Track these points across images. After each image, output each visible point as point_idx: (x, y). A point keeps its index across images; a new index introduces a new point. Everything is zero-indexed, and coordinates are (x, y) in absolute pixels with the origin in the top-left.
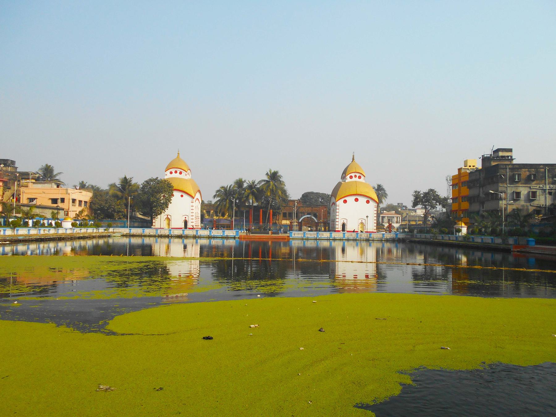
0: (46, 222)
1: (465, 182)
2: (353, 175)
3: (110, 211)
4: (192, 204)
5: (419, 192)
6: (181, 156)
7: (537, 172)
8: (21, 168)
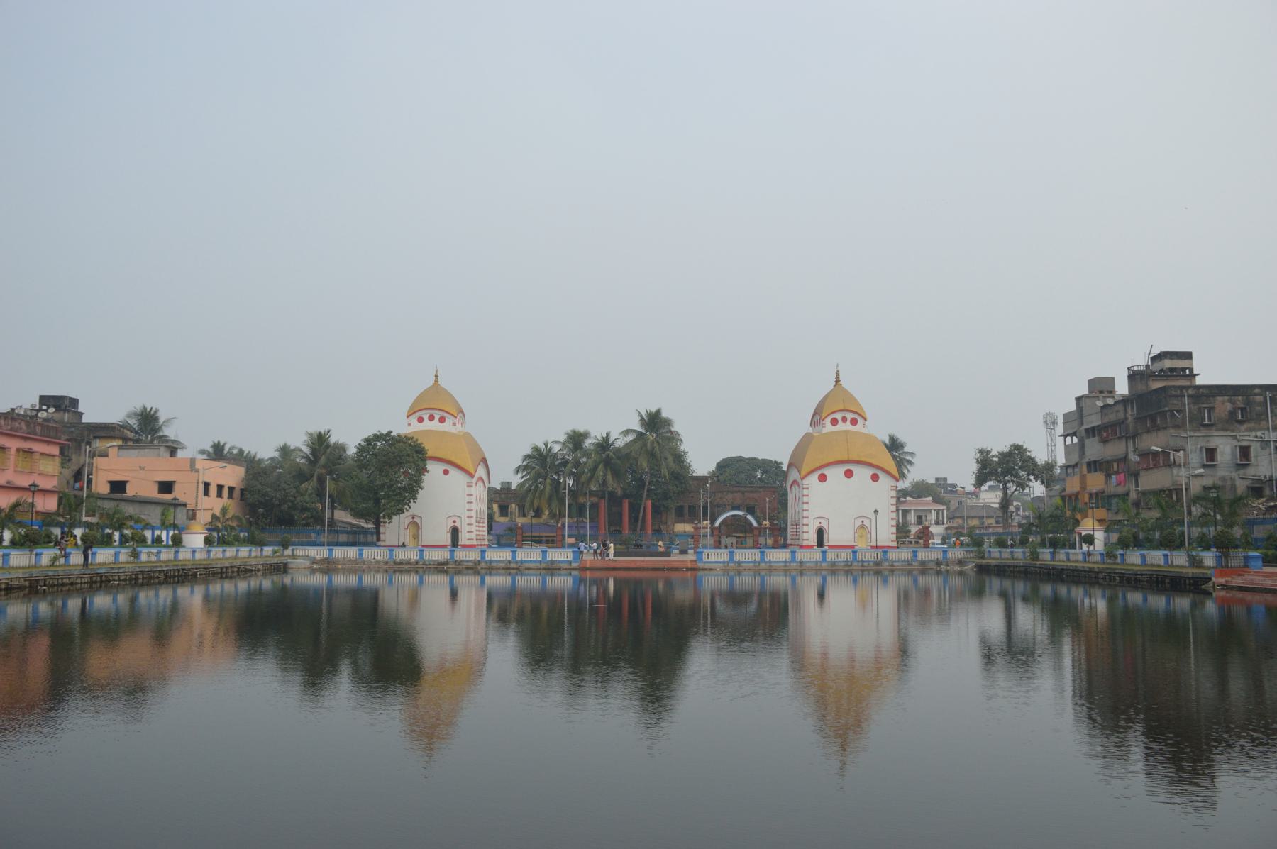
0: (148, 534)
1: (1093, 428)
2: (839, 416)
4: (468, 491)
5: (988, 452)
7: (1249, 403)
8: (92, 414)
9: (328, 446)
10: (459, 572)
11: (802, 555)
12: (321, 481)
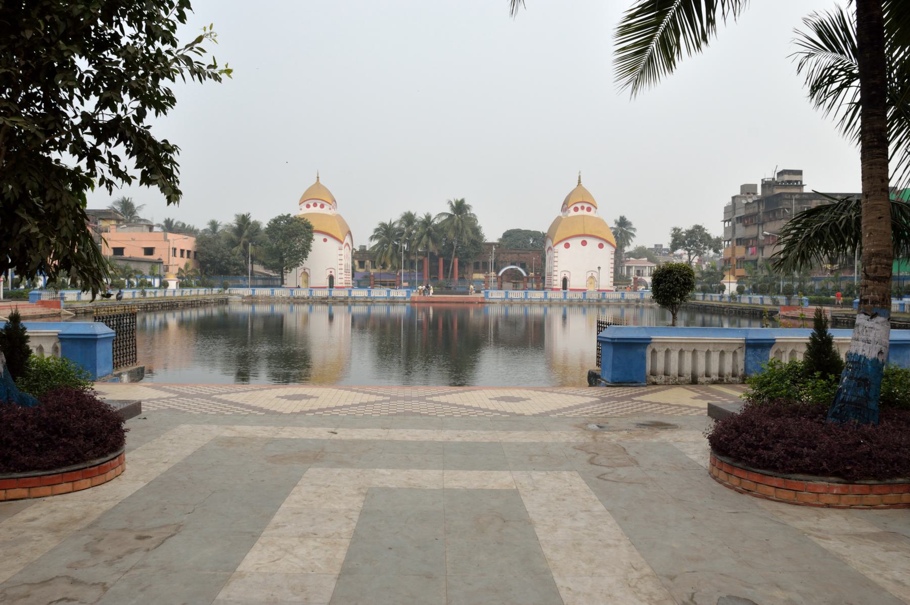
1: (741, 217)
2: (579, 206)
3: (223, 263)
4: (340, 252)
5: (679, 230)
6: (321, 181)
8: (141, 214)
9: (249, 224)
10: (334, 304)
11: (551, 295)
12: (246, 246)
